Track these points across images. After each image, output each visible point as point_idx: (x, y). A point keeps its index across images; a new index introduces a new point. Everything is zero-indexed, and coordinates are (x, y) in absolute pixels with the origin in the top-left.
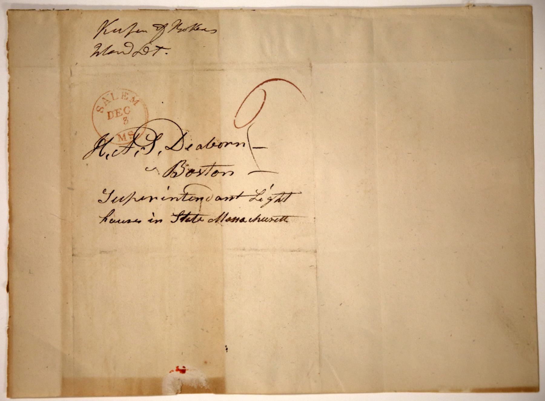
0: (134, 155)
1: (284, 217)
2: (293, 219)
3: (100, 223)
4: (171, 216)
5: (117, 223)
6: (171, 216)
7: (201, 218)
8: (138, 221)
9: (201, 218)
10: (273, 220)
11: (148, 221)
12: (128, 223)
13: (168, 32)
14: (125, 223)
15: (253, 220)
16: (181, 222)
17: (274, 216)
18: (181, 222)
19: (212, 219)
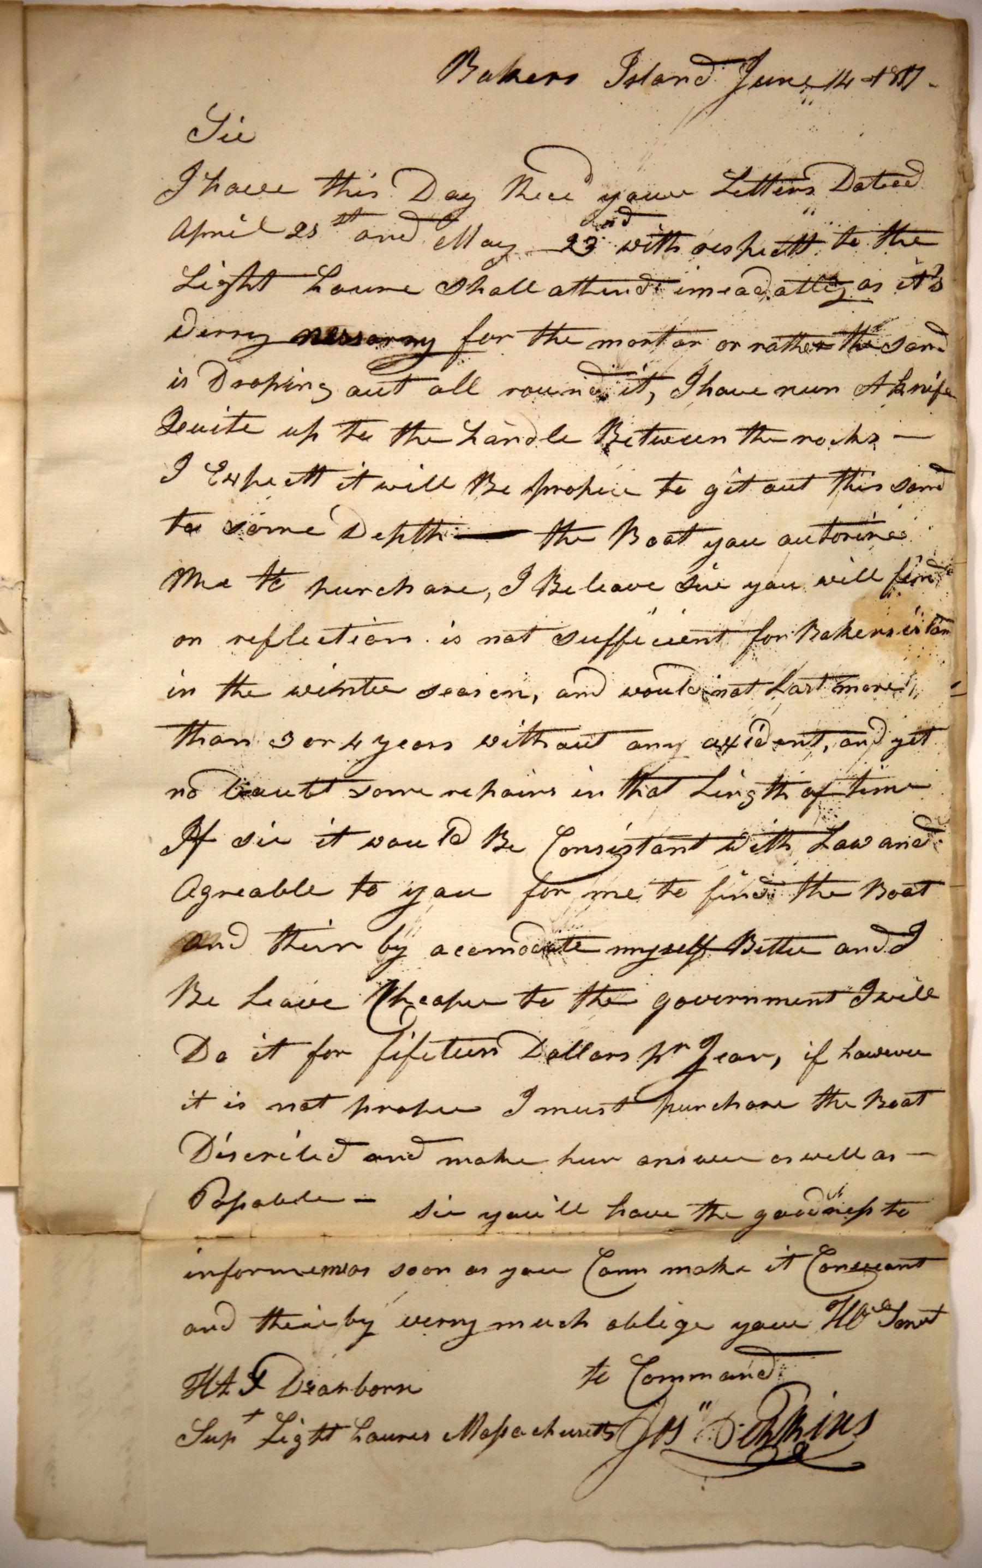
0: (277, 981)
1: (782, 939)
2: (836, 801)
3: (338, 506)
4: (505, 1150)
5: (854, 1157)
6: (505, 1150)
7: (247, 426)
8: (630, 951)
9: (247, 426)
10: (853, 538)
11: (732, 1327)
12: (165, 477)
13: (510, 1416)
14: (263, 1060)
15: (723, 250)
16: (626, 88)
17: (594, 658)
18: (626, 88)
19: (845, 1158)
